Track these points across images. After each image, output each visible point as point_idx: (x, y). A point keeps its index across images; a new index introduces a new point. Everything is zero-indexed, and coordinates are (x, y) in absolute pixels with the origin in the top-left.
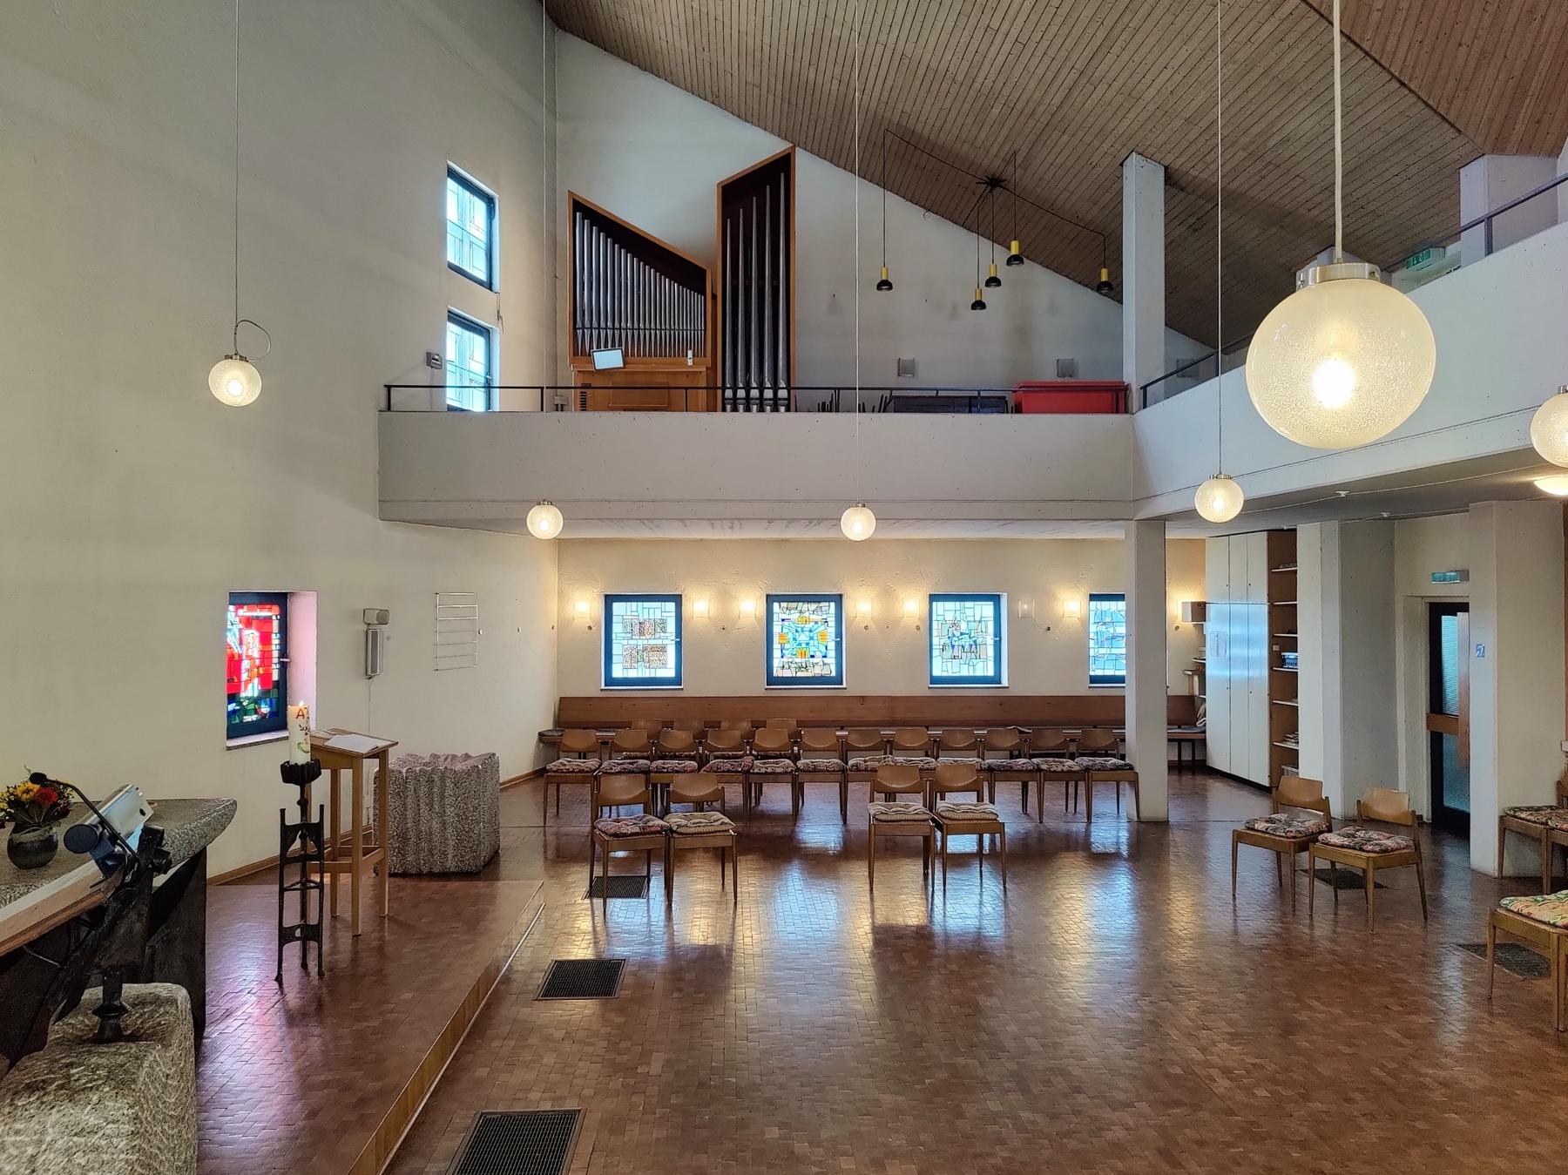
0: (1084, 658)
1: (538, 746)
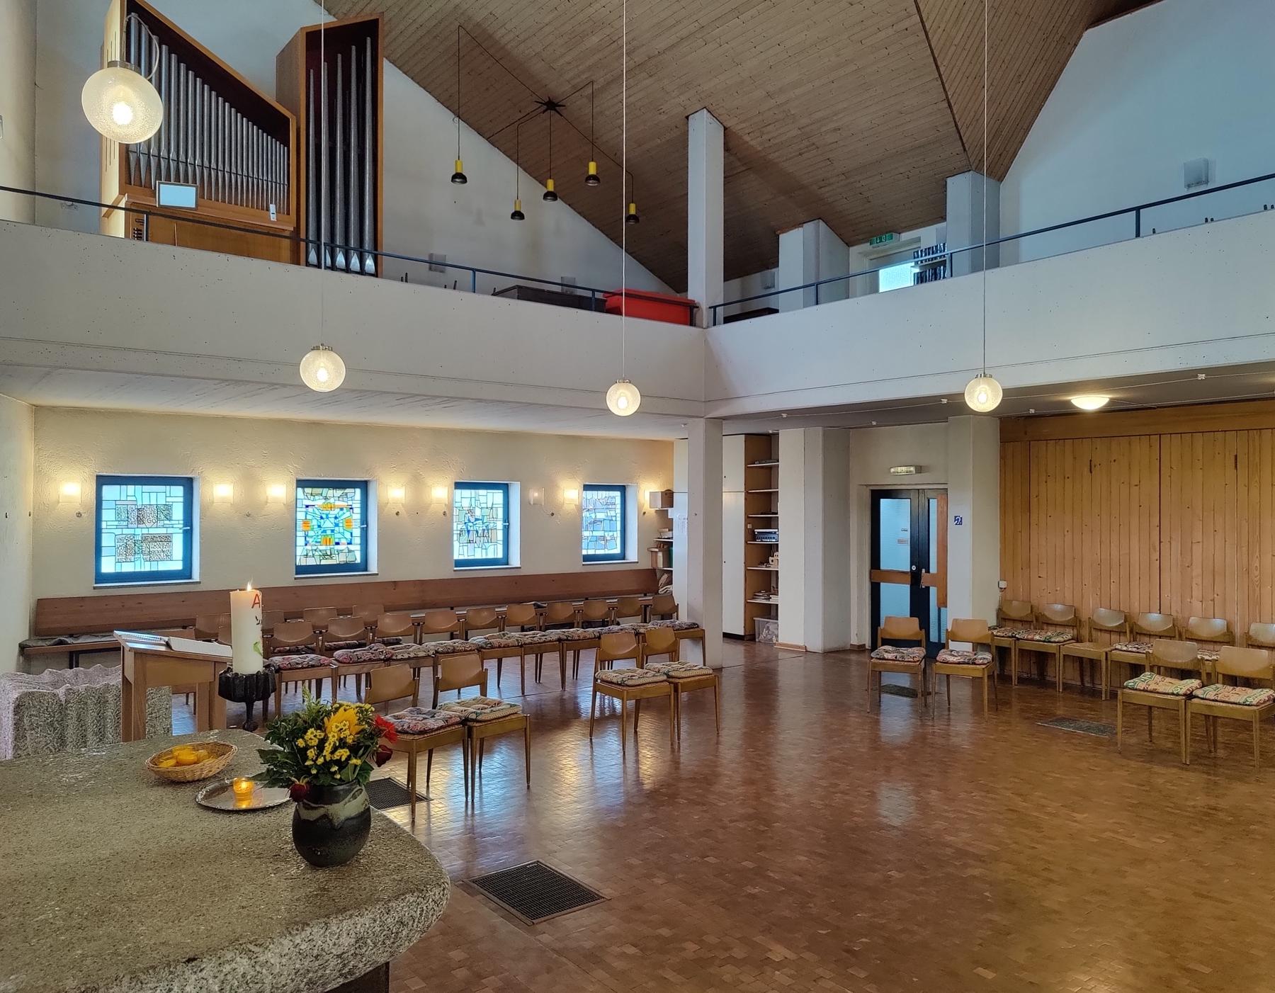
1: (18, 660)
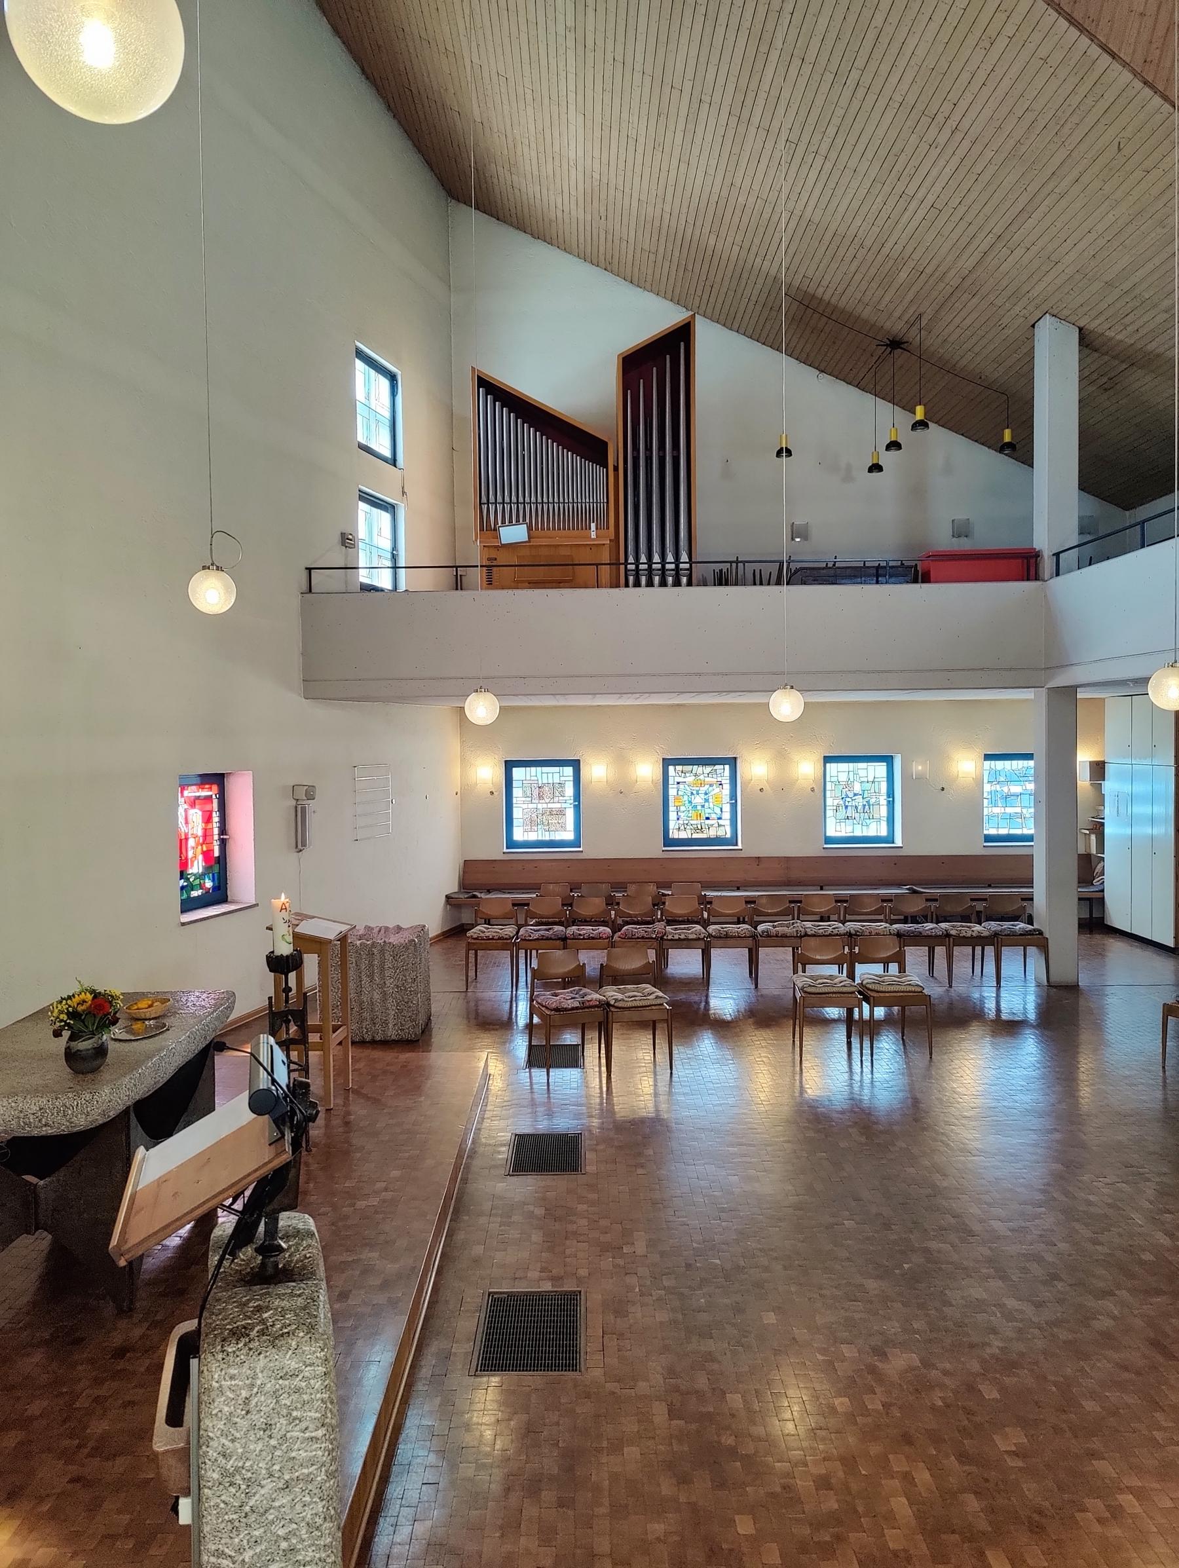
0: (978, 818)
